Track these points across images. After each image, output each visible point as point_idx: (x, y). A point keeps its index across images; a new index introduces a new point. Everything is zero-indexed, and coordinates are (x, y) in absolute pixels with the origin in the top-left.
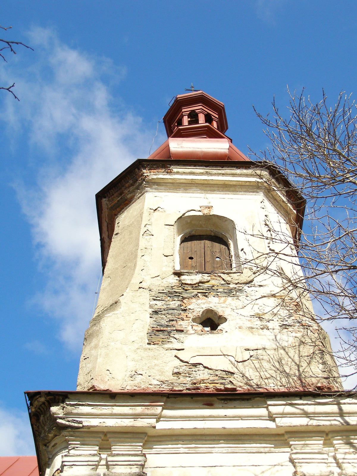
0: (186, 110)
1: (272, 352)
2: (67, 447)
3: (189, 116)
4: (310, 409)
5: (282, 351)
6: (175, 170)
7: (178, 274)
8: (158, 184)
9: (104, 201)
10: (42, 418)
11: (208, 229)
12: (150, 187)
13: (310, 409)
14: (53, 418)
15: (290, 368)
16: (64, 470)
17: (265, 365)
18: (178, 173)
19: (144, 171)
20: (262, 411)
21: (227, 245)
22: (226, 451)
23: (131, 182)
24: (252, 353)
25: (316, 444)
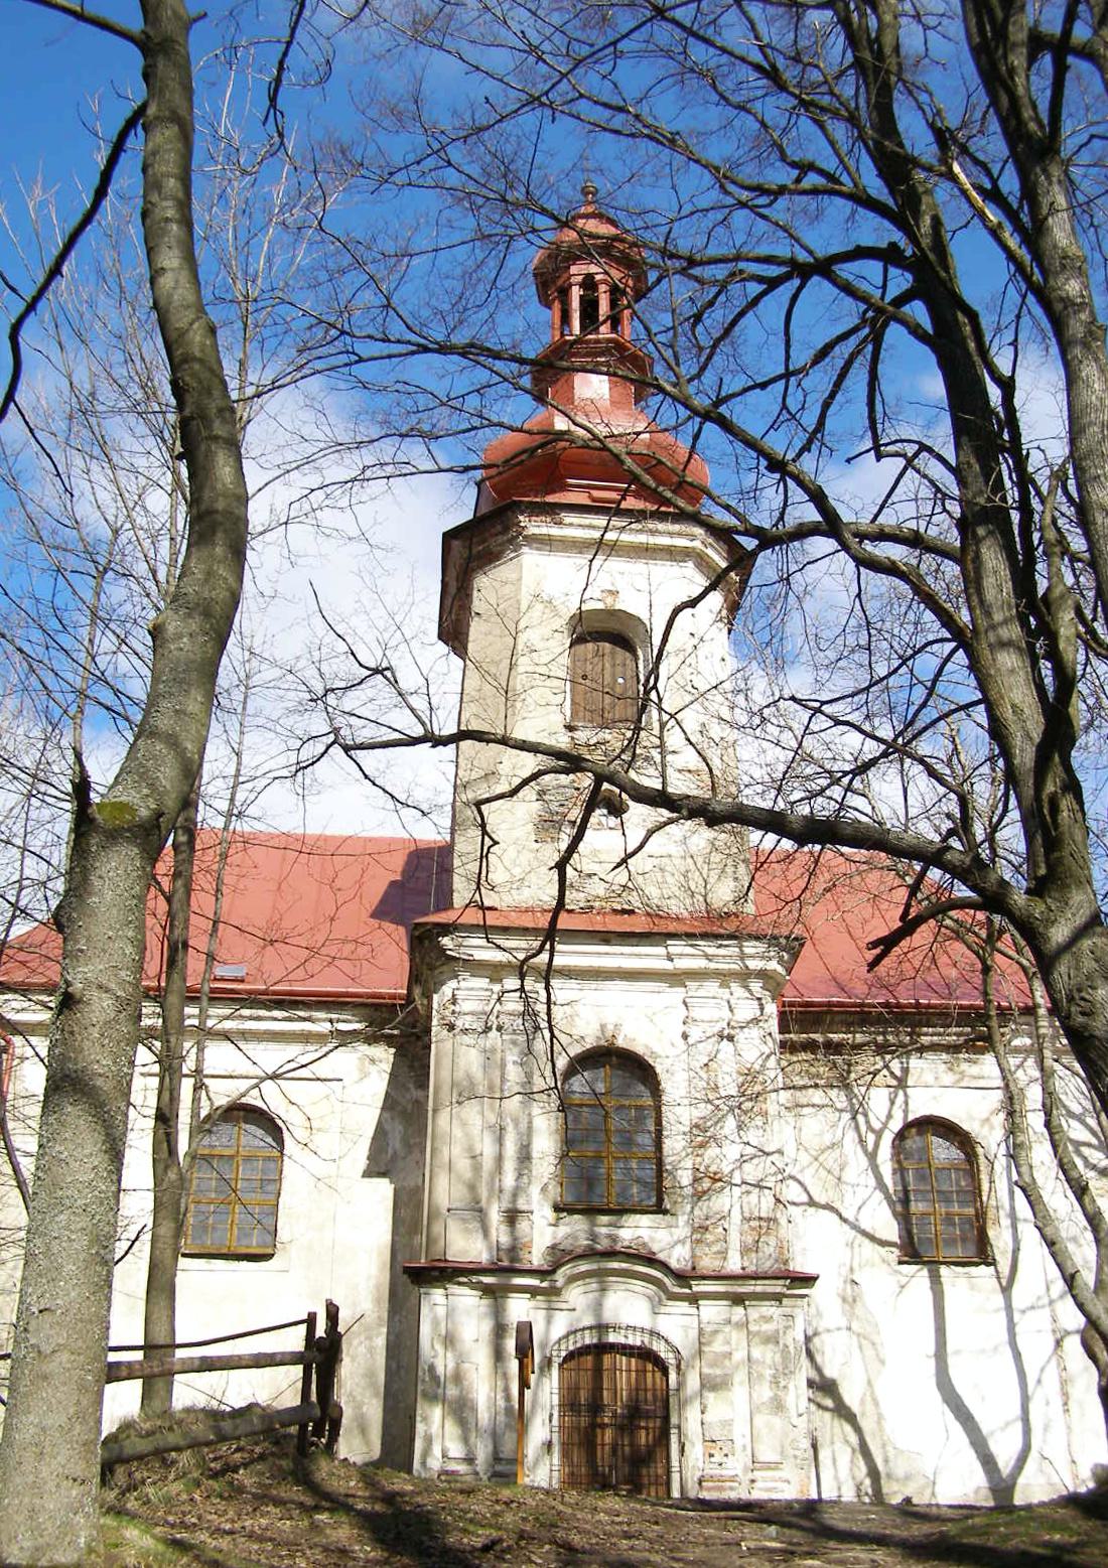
0: (578, 270)
1: (677, 862)
2: (456, 977)
3: (582, 285)
4: (711, 951)
5: (690, 860)
6: (567, 520)
7: (570, 728)
8: (546, 543)
9: (456, 544)
10: (427, 942)
11: (612, 625)
12: (529, 545)
13: (711, 951)
14: (442, 950)
15: (696, 883)
16: (985, 1431)
17: (670, 879)
18: (571, 525)
19: (521, 518)
20: (661, 950)
21: (633, 652)
22: (324, 367)
23: (499, 528)
24: (656, 862)
25: (712, 987)
